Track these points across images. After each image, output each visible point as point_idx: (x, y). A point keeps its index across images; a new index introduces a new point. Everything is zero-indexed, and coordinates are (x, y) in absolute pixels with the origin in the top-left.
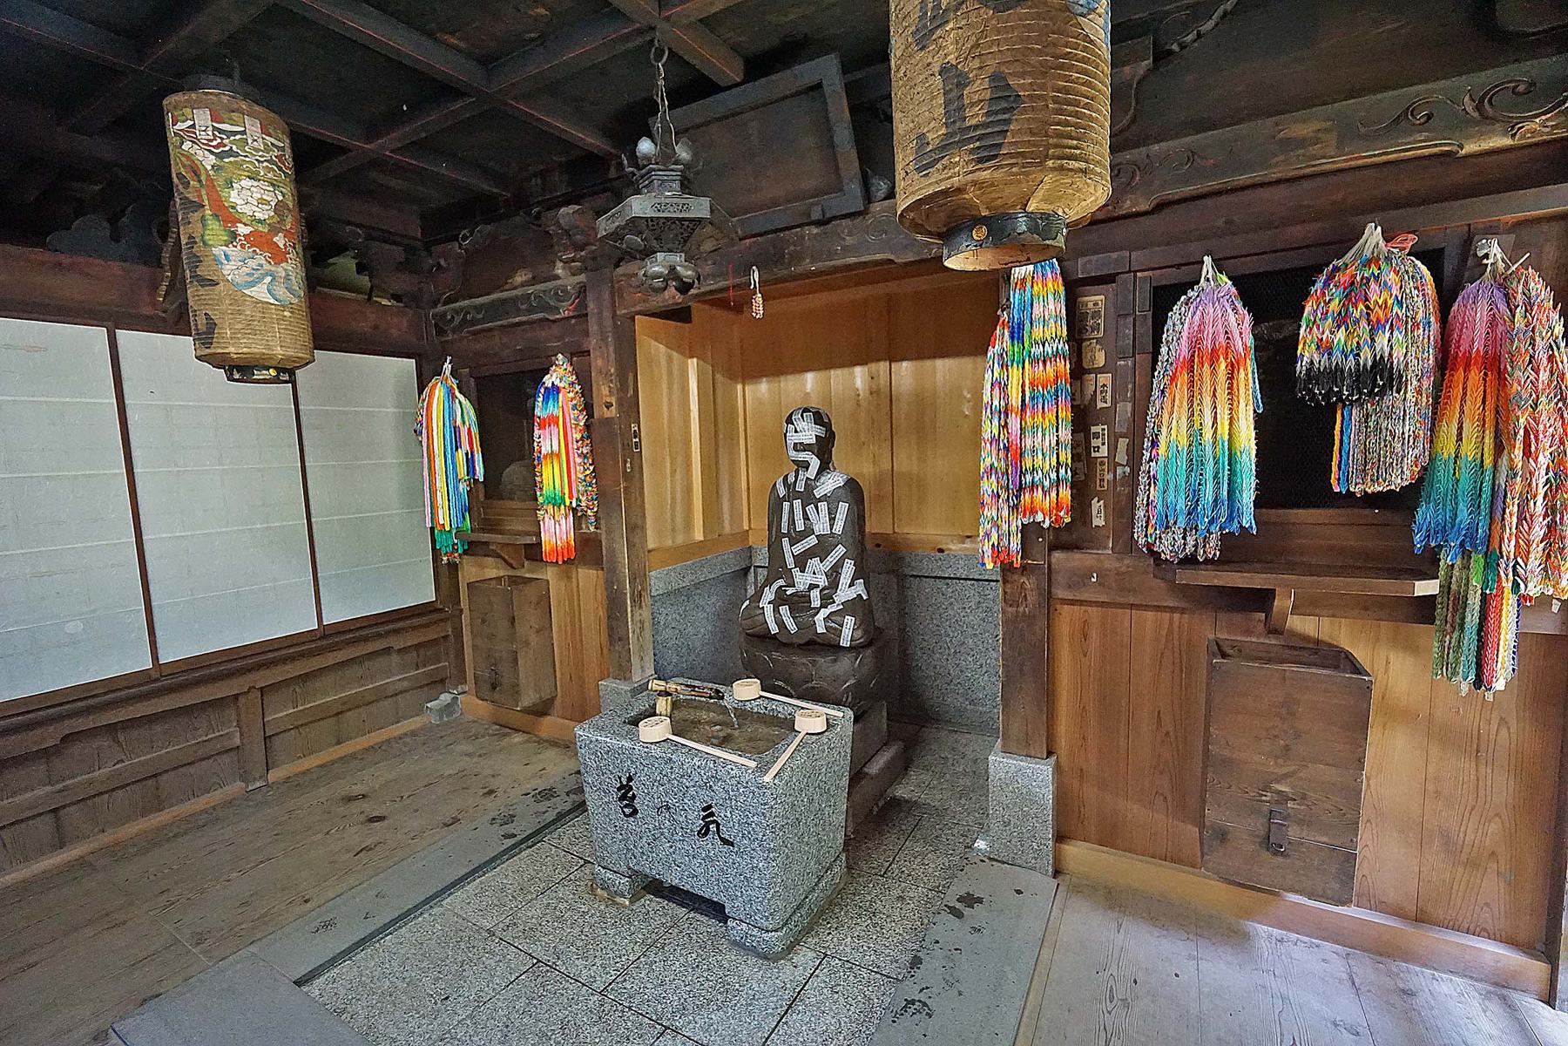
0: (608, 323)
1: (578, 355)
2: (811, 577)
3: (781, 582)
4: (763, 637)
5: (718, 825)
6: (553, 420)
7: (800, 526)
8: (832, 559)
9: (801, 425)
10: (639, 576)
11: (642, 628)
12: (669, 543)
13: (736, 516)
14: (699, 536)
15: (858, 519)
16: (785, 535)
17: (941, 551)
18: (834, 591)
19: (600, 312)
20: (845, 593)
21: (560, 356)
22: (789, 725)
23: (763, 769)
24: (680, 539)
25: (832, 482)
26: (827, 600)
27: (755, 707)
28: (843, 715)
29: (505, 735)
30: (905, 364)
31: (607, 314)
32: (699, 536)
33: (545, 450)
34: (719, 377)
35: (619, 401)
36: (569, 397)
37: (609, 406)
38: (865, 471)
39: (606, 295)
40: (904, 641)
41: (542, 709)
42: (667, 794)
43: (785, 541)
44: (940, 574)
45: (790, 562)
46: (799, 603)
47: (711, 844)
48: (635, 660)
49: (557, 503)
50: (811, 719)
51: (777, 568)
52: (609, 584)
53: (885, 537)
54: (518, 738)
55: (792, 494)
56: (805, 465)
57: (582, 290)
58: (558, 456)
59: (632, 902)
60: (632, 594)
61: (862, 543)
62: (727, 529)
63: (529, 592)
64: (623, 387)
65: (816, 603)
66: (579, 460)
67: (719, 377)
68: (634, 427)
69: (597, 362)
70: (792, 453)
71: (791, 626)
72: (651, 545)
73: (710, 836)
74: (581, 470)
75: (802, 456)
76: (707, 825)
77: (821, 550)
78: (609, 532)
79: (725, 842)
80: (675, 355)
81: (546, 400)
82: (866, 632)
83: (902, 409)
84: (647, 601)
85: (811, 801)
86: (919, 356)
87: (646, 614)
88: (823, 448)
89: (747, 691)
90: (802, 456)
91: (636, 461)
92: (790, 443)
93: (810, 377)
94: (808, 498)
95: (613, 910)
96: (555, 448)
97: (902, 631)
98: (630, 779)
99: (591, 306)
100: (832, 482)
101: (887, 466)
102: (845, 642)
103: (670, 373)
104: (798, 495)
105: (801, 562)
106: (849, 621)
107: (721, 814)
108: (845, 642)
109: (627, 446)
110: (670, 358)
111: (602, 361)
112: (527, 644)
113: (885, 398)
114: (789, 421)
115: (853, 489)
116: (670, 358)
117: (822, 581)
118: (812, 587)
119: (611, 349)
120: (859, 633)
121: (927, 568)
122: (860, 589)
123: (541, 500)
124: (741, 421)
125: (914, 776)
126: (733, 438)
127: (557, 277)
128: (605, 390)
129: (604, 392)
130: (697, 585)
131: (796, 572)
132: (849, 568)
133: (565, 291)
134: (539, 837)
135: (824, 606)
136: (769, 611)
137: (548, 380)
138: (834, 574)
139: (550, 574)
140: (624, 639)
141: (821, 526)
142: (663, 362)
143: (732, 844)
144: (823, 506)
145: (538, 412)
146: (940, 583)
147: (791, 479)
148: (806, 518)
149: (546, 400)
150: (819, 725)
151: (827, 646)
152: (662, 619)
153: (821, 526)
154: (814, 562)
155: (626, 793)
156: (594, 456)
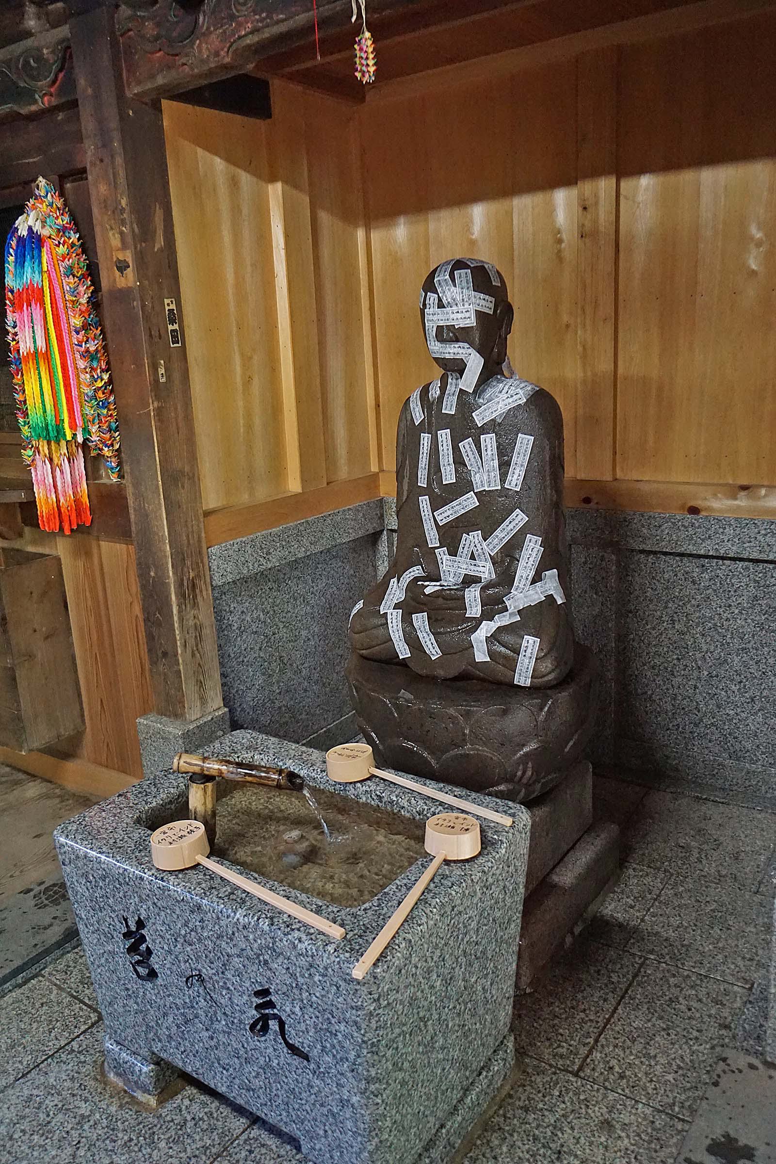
0: (111, 113)
1: (69, 176)
2: (470, 561)
3: (416, 571)
4: (382, 664)
5: (282, 1024)
6: (33, 295)
7: (449, 476)
8: (503, 534)
9: (449, 292)
10: (190, 556)
11: (199, 638)
12: (245, 498)
13: (358, 453)
14: (294, 485)
15: (550, 463)
16: (423, 492)
17: (694, 511)
18: (504, 590)
19: (97, 96)
20: (524, 594)
21: (42, 181)
22: (415, 830)
23: (354, 946)
24: (263, 493)
25: (505, 398)
26: (493, 605)
27: (363, 794)
28: (512, 821)
29: (17, 783)
30: (645, 181)
31: (109, 97)
32: (294, 485)
33: (25, 345)
34: (324, 217)
35: (140, 257)
36: (59, 253)
37: (122, 267)
38: (567, 374)
39: (105, 59)
40: (624, 654)
41: (65, 750)
42: (198, 958)
43: (424, 502)
44: (692, 549)
45: (432, 538)
46: (445, 610)
47: (269, 1045)
48: (189, 688)
49: (53, 435)
50: (460, 831)
51: (413, 551)
52: (143, 569)
53: (599, 487)
54: (33, 790)
55: (435, 419)
56: (458, 367)
57: (66, 54)
58: (47, 356)
59: (161, 1102)
60: (180, 584)
61: (557, 505)
62: (344, 472)
63: (30, 578)
64: (145, 233)
65: (474, 610)
66: (82, 364)
67: (324, 217)
68: (169, 304)
69: (99, 188)
70: (436, 348)
71: (433, 650)
72: (211, 499)
73: (270, 1036)
74: (88, 381)
75: (453, 351)
76: (265, 1019)
77: (485, 518)
78: (136, 485)
79: (294, 1050)
80: (245, 178)
81: (20, 262)
82: (559, 663)
83: (637, 260)
84: (205, 596)
85: (448, 981)
86: (669, 163)
87: (205, 615)
88: (492, 335)
89: (349, 764)
90: (453, 351)
91: (176, 365)
92: (431, 327)
93: (479, 214)
94: (463, 427)
95: (129, 1115)
96: (41, 343)
97: (622, 638)
98: (140, 924)
99: (82, 82)
100: (505, 398)
101: (605, 366)
102: (523, 677)
103: (236, 210)
104: (447, 422)
105: (451, 536)
106: (531, 644)
107: (284, 1007)
108: (523, 677)
109: (156, 337)
110: (234, 183)
111: (107, 187)
112: (31, 656)
113: (606, 243)
114: (429, 286)
115: (543, 405)
116: (234, 183)
117: (486, 571)
118: (469, 581)
119: (119, 160)
120: (547, 665)
121: (668, 537)
122: (551, 585)
123: (26, 431)
124: (364, 291)
125: (636, 878)
126: (350, 318)
127: (28, 34)
128: (115, 241)
129: (112, 243)
130: (294, 564)
131: (442, 554)
132: (532, 550)
133: (39, 59)
134: (33, 970)
135: (488, 615)
136: (395, 619)
137: (23, 225)
138: (506, 561)
139: (61, 548)
140: (169, 655)
141: (485, 477)
142: (223, 190)
143: (306, 1058)
144: (489, 441)
145: (10, 281)
146: (689, 565)
147: (435, 392)
148: (459, 461)
149: (20, 262)
150: (466, 846)
151: (489, 684)
152: (234, 620)
153: (485, 477)
154: (472, 540)
155: (135, 940)
156: (107, 357)
